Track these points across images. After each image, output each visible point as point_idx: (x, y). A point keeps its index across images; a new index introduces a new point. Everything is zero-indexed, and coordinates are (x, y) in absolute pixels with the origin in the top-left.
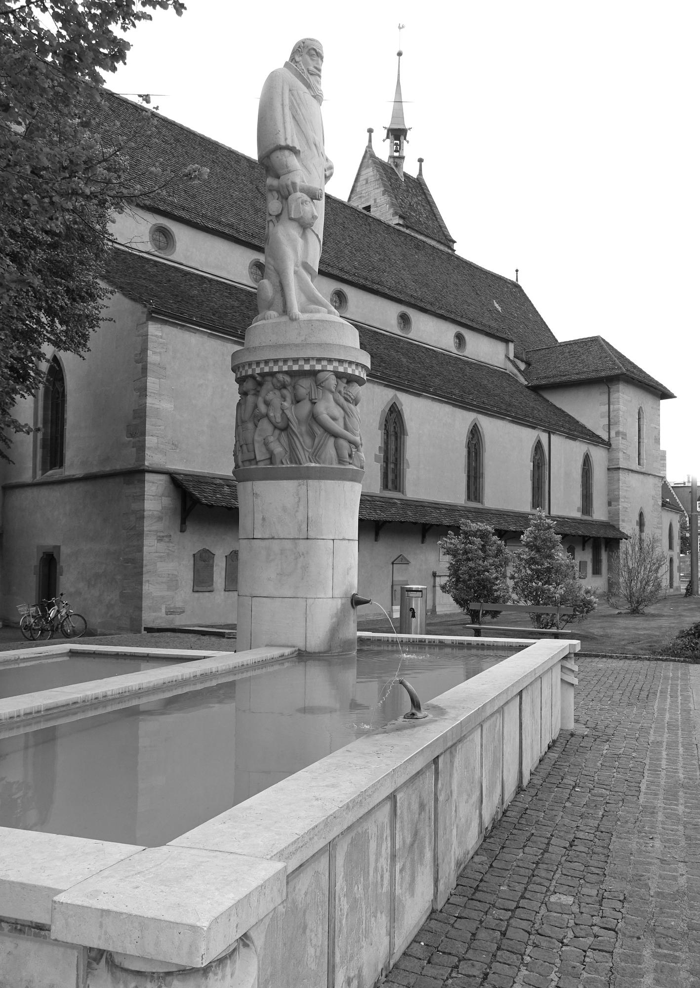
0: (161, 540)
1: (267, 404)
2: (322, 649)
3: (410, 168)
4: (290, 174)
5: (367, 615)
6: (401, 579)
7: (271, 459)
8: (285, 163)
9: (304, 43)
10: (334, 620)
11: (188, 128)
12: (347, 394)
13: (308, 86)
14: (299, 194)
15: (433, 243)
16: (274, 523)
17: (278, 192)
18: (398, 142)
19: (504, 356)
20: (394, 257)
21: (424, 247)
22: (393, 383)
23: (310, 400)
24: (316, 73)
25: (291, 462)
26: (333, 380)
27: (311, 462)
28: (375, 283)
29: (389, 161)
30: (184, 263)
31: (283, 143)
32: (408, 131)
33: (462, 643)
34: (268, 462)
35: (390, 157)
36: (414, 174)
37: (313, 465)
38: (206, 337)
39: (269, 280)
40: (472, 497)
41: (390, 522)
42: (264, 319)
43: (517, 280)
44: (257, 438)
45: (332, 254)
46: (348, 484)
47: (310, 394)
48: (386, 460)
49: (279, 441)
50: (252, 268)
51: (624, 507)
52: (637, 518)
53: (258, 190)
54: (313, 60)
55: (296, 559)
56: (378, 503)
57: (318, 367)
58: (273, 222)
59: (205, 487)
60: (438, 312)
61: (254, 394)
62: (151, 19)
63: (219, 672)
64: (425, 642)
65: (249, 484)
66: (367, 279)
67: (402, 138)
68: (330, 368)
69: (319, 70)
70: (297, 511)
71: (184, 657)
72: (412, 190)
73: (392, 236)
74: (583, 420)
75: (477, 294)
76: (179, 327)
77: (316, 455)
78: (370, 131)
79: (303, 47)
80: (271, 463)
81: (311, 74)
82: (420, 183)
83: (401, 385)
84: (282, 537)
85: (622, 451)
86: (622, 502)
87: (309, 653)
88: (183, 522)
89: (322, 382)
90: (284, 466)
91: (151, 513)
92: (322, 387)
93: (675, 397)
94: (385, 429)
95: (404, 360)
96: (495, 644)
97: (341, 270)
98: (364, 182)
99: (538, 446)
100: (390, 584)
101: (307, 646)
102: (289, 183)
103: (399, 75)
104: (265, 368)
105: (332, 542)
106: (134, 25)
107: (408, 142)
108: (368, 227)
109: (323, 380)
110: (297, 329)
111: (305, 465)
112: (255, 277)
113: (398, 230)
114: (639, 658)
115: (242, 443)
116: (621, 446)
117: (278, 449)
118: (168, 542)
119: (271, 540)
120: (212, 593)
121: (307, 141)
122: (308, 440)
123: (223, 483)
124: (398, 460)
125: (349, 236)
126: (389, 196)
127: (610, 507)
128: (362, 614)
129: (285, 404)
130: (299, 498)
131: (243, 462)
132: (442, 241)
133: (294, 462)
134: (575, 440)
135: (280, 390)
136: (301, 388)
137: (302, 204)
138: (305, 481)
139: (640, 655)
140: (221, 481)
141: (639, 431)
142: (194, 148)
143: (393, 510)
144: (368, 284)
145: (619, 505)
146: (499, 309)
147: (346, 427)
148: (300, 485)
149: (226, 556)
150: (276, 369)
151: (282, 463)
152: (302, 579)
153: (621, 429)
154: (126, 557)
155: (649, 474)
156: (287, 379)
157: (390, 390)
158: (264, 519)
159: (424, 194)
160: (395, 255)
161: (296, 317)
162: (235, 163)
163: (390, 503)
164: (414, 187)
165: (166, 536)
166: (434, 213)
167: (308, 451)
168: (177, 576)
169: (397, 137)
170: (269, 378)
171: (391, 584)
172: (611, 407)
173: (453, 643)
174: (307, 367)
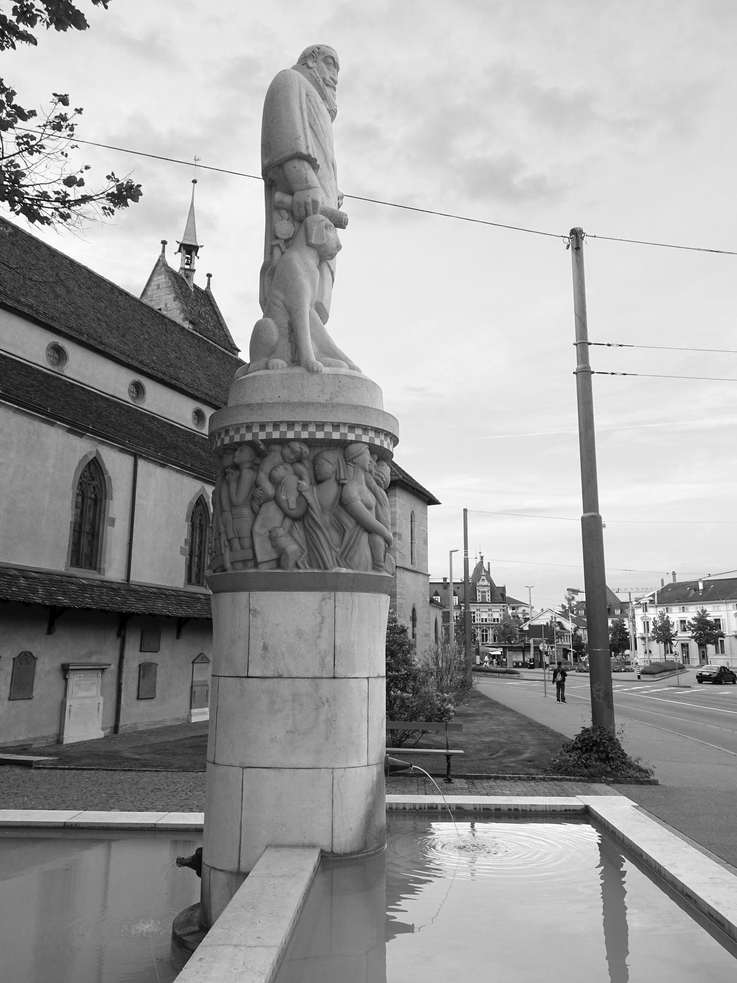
1: (277, 483)
2: (356, 846)
3: (199, 280)
4: (310, 191)
5: (164, 720)
6: (201, 679)
8: (305, 176)
9: (319, 48)
12: (379, 476)
13: (324, 98)
14: (322, 217)
15: (223, 349)
16: (282, 654)
17: (291, 212)
18: (189, 256)
20: (189, 356)
21: (215, 351)
22: (202, 475)
23: (336, 480)
24: (332, 84)
25: (311, 566)
27: (339, 565)
28: (172, 378)
29: (179, 271)
31: (304, 151)
32: (200, 248)
33: (488, 809)
34: (274, 564)
35: (182, 268)
36: (203, 286)
38: (12, 412)
39: (273, 319)
41: (196, 619)
42: (267, 368)
45: (132, 346)
46: (364, 598)
47: (337, 472)
48: (191, 555)
49: (292, 536)
50: (49, 350)
51: (400, 603)
52: (411, 614)
54: (329, 69)
55: (317, 708)
56: (183, 598)
57: (351, 437)
58: (280, 247)
61: (251, 468)
62: (35, 43)
64: (437, 808)
65: (243, 596)
66: (165, 374)
67: (193, 253)
69: (336, 83)
70: (319, 637)
71: (33, 825)
72: (201, 300)
73: (187, 338)
77: (345, 558)
78: (164, 243)
79: (319, 53)
80: (279, 566)
81: (327, 85)
82: (208, 295)
83: (210, 478)
84: (295, 675)
85: (398, 551)
87: (337, 855)
89: (355, 457)
90: (301, 571)
92: (354, 463)
93: (440, 503)
94: (191, 521)
95: (203, 454)
96: (533, 809)
97: (141, 362)
98: (156, 287)
100: (189, 685)
102: (310, 200)
103: (193, 199)
104: (274, 433)
105: (366, 681)
106: (14, 46)
107: (198, 258)
108: (164, 326)
109: (356, 455)
110: (319, 385)
111: (334, 571)
112: (52, 359)
113: (192, 333)
114: (534, 779)
116: (398, 546)
117: (292, 548)
119: (276, 680)
121: (326, 157)
122: (335, 536)
123: (19, 574)
124: (203, 553)
125: (147, 332)
126: (180, 302)
128: (160, 719)
130: (323, 618)
131: (232, 563)
132: (228, 349)
133: (314, 564)
135: (292, 464)
136: (327, 463)
137: (326, 228)
138: (333, 593)
139: (534, 775)
140: (16, 572)
141: (411, 532)
143: (199, 606)
144: (166, 378)
145: (396, 601)
147: (378, 517)
148: (324, 599)
149: (14, 659)
150: (290, 435)
152: (327, 739)
153: (397, 531)
155: (420, 573)
157: (198, 482)
158: (265, 648)
159: (212, 305)
160: (190, 354)
161: (318, 368)
162: (36, 249)
163: (194, 598)
164: (202, 298)
166: (221, 324)
167: (335, 551)
169: (189, 253)
170: (277, 448)
171: (190, 685)
173: (475, 809)
174: (336, 436)
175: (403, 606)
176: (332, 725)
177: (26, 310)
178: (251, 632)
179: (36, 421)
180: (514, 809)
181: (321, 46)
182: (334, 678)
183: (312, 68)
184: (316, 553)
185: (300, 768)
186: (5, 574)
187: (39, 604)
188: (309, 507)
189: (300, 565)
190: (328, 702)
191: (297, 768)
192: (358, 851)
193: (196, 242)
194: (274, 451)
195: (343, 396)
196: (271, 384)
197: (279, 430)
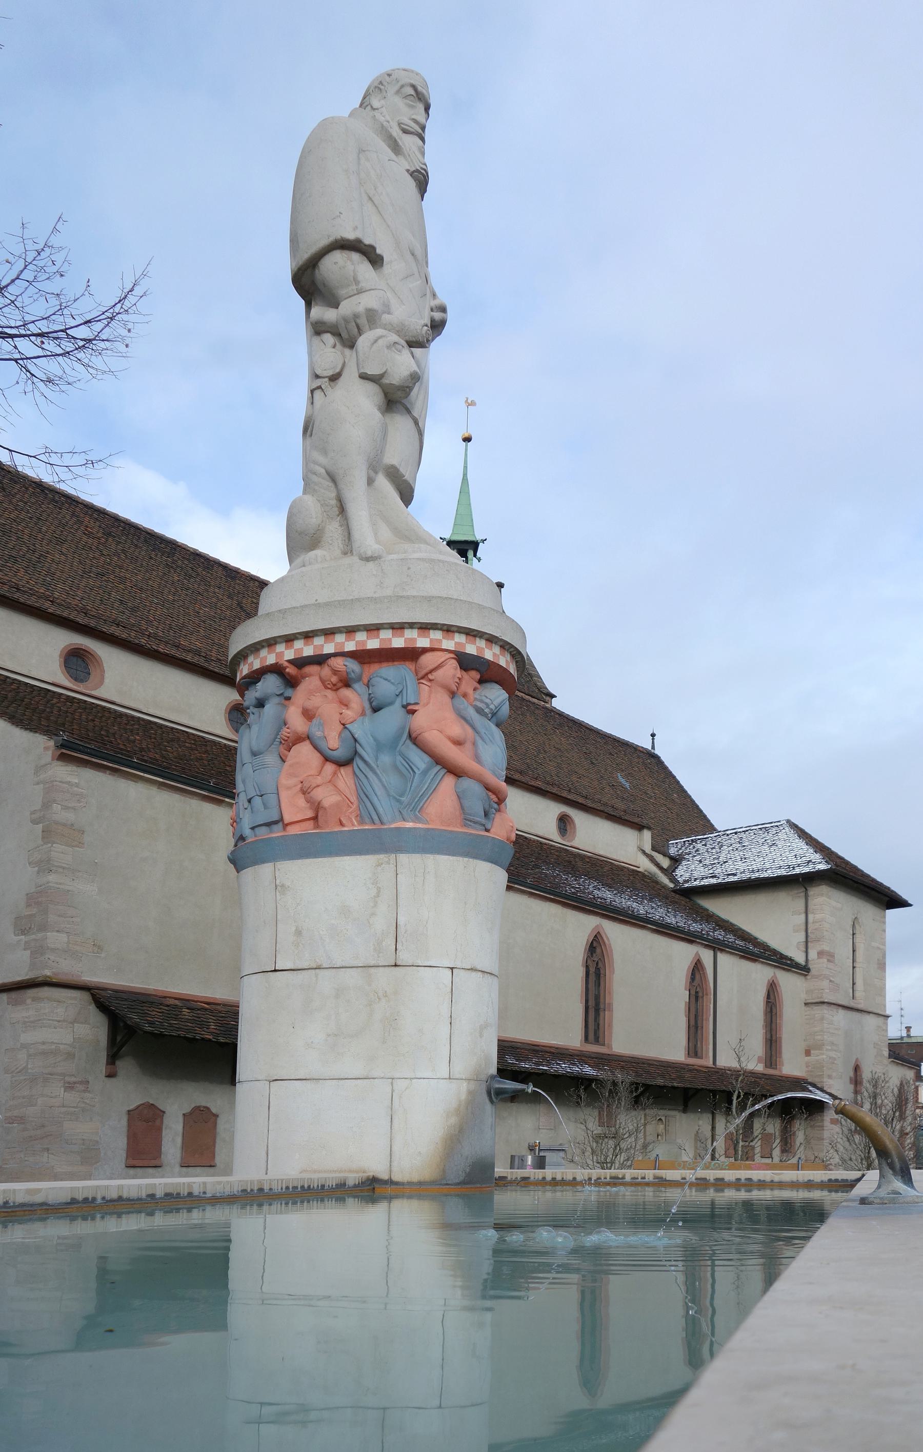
0: (72, 1088)
7: (315, 818)
9: (389, 75)
10: (453, 1120)
11: (127, 520)
18: (464, 559)
19: (636, 848)
26: (451, 670)
30: (118, 701)
37: (410, 825)
40: (591, 1036)
43: (653, 747)
44: (285, 781)
53: (241, 608)
57: (423, 642)
59: (149, 1009)
60: (533, 783)
63: (208, 1195)
65: (266, 869)
68: (449, 644)
70: (373, 914)
74: (763, 935)
75: (592, 763)
76: (108, 772)
86: (827, 1050)
88: (113, 1057)
90: (346, 829)
91: (53, 1047)
93: (910, 905)
99: (697, 968)
101: (394, 1169)
115: (252, 793)
118: (84, 1091)
120: (159, 1169)
123: (181, 1005)
127: (809, 1058)
129: (349, 714)
130: (379, 890)
134: (754, 961)
140: (177, 1002)
142: (136, 546)
146: (627, 785)
148: (379, 865)
149: (184, 1114)
150: (329, 649)
151: (342, 824)
154: (8, 1115)
155: (869, 1013)
156: (353, 666)
158: (298, 933)
165: (81, 1083)
168: (97, 1142)
170: (312, 669)
172: (811, 917)
175: (835, 1062)
176: (391, 1025)
177: (189, 658)
178: (278, 914)
179: (193, 799)
180: (746, 1179)
181: (393, 70)
182: (396, 965)
183: (377, 109)
184: (369, 804)
185: (346, 1079)
186: (161, 1004)
187: (210, 1040)
188: (357, 745)
189: (344, 822)
190: (386, 996)
191: (342, 1079)
192: (430, 1182)
193: (474, 535)
194: (309, 675)
195: (413, 588)
196: (305, 585)
197: (313, 644)
